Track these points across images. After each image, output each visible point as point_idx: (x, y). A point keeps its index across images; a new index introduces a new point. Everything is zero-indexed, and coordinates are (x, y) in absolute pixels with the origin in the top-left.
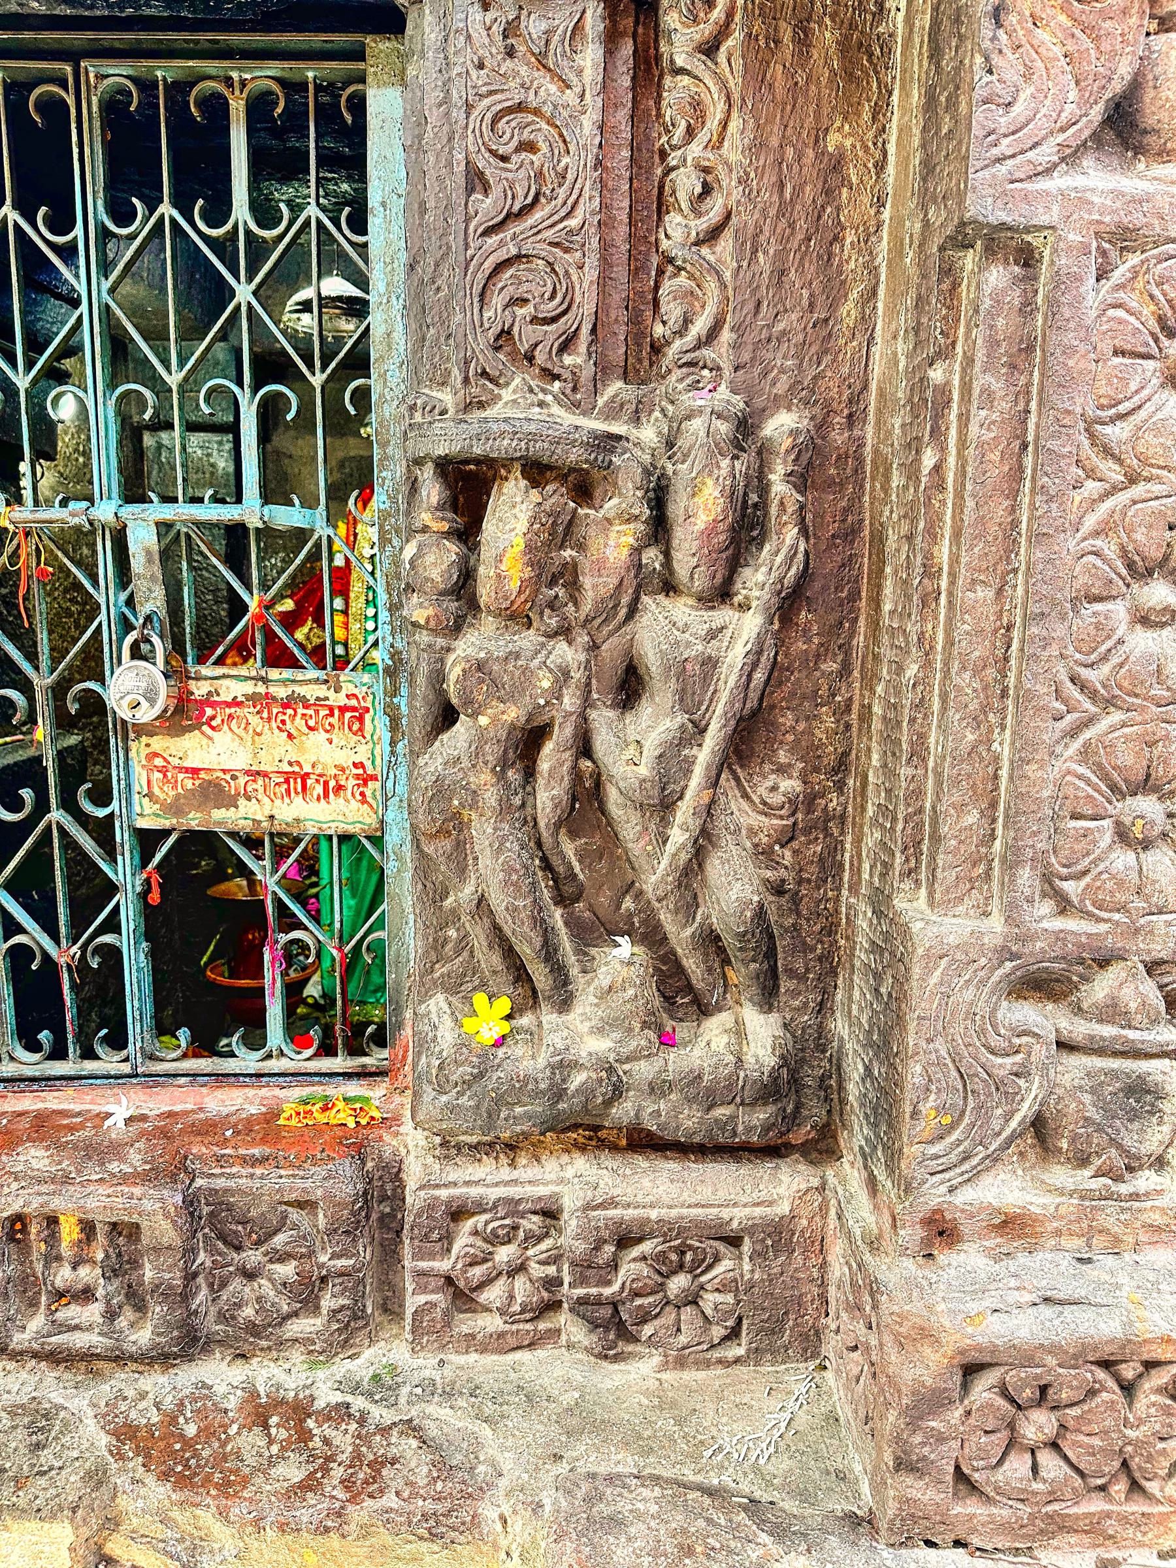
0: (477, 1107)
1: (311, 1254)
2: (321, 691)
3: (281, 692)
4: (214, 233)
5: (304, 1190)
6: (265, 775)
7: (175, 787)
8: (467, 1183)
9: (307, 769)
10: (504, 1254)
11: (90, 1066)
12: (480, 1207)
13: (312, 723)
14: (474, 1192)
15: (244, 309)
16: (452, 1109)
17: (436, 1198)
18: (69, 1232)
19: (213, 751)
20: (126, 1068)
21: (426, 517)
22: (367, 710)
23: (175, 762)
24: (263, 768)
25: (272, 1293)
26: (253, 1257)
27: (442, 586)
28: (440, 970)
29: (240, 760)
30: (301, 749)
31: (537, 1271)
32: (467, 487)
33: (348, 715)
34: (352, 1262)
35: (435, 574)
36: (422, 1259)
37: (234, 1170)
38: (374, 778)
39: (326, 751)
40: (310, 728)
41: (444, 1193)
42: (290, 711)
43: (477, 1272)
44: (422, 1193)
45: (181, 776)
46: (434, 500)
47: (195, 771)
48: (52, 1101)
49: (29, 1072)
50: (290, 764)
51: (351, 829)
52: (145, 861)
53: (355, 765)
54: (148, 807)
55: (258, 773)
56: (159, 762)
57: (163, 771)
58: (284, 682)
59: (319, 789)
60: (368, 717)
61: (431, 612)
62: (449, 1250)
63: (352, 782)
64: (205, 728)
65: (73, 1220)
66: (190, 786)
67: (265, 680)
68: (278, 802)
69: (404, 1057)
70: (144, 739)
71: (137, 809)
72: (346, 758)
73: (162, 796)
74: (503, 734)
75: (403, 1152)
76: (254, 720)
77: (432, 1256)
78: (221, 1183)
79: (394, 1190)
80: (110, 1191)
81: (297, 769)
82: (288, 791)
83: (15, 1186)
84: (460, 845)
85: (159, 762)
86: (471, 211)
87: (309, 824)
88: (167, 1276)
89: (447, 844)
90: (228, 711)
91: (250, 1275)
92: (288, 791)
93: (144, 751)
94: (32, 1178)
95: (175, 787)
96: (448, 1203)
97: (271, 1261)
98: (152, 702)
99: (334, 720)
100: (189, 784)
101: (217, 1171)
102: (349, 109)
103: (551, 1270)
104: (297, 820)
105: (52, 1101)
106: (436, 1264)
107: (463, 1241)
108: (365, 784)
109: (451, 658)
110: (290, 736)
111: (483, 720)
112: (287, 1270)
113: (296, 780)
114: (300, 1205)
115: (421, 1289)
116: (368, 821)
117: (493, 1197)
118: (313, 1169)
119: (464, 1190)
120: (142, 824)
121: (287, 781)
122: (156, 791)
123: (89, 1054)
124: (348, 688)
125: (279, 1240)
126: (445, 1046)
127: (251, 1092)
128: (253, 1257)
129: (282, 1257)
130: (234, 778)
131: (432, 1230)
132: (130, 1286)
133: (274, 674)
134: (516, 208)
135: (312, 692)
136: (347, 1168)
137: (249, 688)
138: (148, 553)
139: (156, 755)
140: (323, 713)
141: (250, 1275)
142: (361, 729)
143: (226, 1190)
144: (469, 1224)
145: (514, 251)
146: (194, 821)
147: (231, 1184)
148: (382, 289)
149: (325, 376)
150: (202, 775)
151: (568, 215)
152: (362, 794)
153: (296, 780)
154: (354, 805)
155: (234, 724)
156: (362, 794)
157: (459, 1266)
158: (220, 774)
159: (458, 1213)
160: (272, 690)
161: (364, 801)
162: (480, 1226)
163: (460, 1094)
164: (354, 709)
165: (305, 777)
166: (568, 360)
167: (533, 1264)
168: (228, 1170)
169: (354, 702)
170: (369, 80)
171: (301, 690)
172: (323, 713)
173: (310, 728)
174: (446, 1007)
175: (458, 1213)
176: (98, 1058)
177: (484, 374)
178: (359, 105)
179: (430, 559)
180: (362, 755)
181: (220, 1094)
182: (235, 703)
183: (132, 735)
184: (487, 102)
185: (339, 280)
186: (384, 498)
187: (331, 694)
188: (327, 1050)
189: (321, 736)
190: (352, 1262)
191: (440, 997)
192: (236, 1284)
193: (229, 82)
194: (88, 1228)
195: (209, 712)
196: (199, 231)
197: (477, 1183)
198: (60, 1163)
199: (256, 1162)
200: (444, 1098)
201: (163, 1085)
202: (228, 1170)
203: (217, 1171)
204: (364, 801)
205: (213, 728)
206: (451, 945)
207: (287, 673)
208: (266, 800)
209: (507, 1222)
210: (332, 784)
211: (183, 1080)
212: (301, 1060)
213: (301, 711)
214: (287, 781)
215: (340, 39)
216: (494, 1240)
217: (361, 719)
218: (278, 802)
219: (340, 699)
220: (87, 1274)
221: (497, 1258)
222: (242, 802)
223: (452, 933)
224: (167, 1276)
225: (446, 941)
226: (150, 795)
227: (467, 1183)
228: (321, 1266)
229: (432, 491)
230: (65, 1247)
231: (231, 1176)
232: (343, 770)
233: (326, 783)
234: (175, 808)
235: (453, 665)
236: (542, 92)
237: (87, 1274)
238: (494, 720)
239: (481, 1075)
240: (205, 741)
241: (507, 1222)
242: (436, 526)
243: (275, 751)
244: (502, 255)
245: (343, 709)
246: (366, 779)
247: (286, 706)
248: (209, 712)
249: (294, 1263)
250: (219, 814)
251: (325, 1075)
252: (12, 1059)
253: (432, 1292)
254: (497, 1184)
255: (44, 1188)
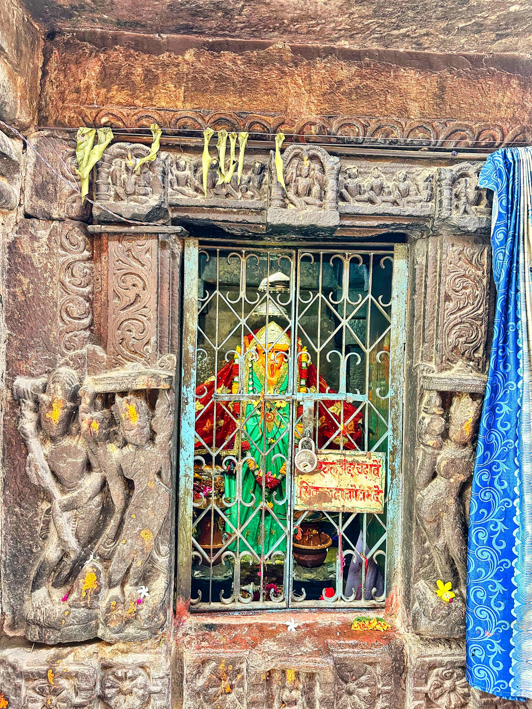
0: (447, 626)
1: (375, 685)
2: (364, 459)
3: (350, 459)
4: (336, 303)
5: (374, 658)
6: (342, 490)
7: (309, 494)
8: (435, 655)
9: (358, 488)
10: (448, 684)
11: (269, 604)
12: (441, 665)
13: (360, 471)
14: (439, 658)
15: (344, 328)
16: (438, 627)
17: (425, 661)
18: (290, 676)
19: (324, 480)
20: (284, 604)
21: (435, 410)
22: (380, 466)
23: (310, 485)
24: (341, 487)
25: (359, 701)
26: (352, 686)
27: (438, 433)
28: (422, 571)
29: (334, 484)
30: (356, 480)
31: (460, 690)
32: (447, 398)
33: (373, 468)
34: (390, 687)
35: (436, 429)
36: (417, 686)
37: (347, 650)
38: (381, 492)
39: (366, 481)
40: (359, 472)
41: (427, 659)
42: (352, 466)
43: (438, 691)
44: (419, 659)
45: (312, 490)
46: (438, 404)
47: (317, 488)
48: (259, 619)
49: (247, 607)
50: (351, 486)
51: (372, 511)
52: (295, 521)
53: (375, 487)
54: (300, 502)
55: (340, 489)
56: (305, 485)
57: (306, 488)
58: (351, 456)
59: (361, 496)
60: (380, 469)
61: (435, 442)
62: (426, 682)
63: (374, 493)
64: (322, 472)
65: (293, 672)
66: (315, 494)
67: (344, 455)
68: (346, 500)
69: (392, 602)
70: (300, 476)
71: (296, 503)
72: (372, 484)
73: (305, 498)
74: (458, 485)
75: (404, 642)
76: (340, 469)
77: (421, 685)
78: (342, 655)
79: (400, 657)
80: (307, 660)
81: (354, 488)
82: (350, 496)
83: (269, 658)
84: (438, 526)
85: (305, 485)
86: (446, 308)
87: (357, 509)
88: (328, 695)
89: (435, 525)
90: (331, 466)
91: (350, 693)
92: (350, 496)
93: (300, 480)
94: (276, 654)
95: (309, 494)
96: (429, 664)
97: (359, 687)
98: (312, 465)
99: (368, 470)
100: (315, 493)
101: (341, 650)
102: (384, 264)
103: (466, 690)
104: (353, 508)
105: (259, 619)
106: (423, 688)
107: (432, 680)
108: (378, 494)
109: (439, 458)
110: (352, 475)
111: (452, 480)
112: (365, 691)
113: (353, 492)
114: (370, 664)
115: (416, 699)
116: (379, 508)
117: (446, 661)
118: (376, 649)
119: (435, 658)
120: (297, 508)
121: (350, 492)
122: (303, 495)
123: (268, 598)
124: (374, 458)
125: (363, 678)
126: (433, 602)
127: (333, 615)
128: (352, 686)
129: (362, 686)
130: (331, 491)
131: (422, 674)
132: (309, 699)
133: (348, 452)
134: (461, 306)
135: (361, 459)
136: (385, 648)
137: (338, 457)
138: (310, 410)
139: (304, 482)
140: (364, 467)
141: (350, 693)
142: (378, 473)
143: (345, 658)
144: (435, 671)
145: (460, 321)
146: (316, 507)
147: (346, 655)
148: (396, 323)
149: (371, 350)
150: (320, 490)
151: (478, 309)
152: (377, 498)
153: (353, 492)
154: (374, 502)
155: (332, 471)
156: (377, 498)
157: (432, 689)
158: (326, 490)
159: (432, 667)
160: (346, 458)
161: (378, 501)
162: (440, 672)
163: (441, 621)
164: (375, 466)
165: (356, 491)
166: (476, 355)
167: (458, 688)
168: (344, 650)
169: (375, 463)
170: (395, 257)
171: (357, 458)
172: (364, 467)
173: (359, 472)
174: (426, 586)
175: (432, 667)
176: (271, 600)
177: (448, 360)
178: (389, 265)
179: (435, 423)
180: (378, 483)
181: (322, 616)
182: (333, 463)
183: (296, 475)
184: (452, 274)
185: (280, 273)
186: (393, 392)
187: (367, 460)
188: (358, 598)
189: (363, 475)
190: (390, 687)
191: (422, 581)
192: (345, 696)
193: (344, 255)
194: (297, 674)
195: (324, 466)
196: (329, 302)
197: (439, 655)
198: (283, 648)
199: (355, 646)
200: (434, 623)
201: (298, 612)
202: (344, 650)
203: (341, 650)
204: (378, 501)
205: (325, 472)
206: (426, 561)
207: (352, 452)
208: (342, 500)
209: (450, 671)
210: (366, 494)
211: (306, 610)
212: (351, 601)
213: (356, 466)
214: (350, 492)
215: (347, 222)
216: (445, 678)
217: (378, 469)
218: (346, 500)
219: (371, 462)
220: (296, 694)
221: (445, 685)
222: (333, 500)
223: (427, 556)
224: (328, 695)
225: (425, 559)
226: (300, 497)
227: (435, 655)
228: (379, 689)
229: (437, 401)
230: (288, 683)
231: (346, 652)
232: (370, 488)
233: (364, 493)
234: (309, 503)
235: (442, 460)
236: (471, 272)
237: (296, 694)
238: (456, 480)
239: (449, 614)
240: (322, 477)
241: (450, 671)
242: (438, 413)
243: (347, 481)
244: (456, 322)
245: (371, 466)
246: (379, 492)
247: (351, 464)
248: (324, 466)
249: (368, 688)
250: (325, 505)
251: (361, 608)
252: (239, 601)
253: (421, 700)
254: (446, 656)
255: (283, 659)
